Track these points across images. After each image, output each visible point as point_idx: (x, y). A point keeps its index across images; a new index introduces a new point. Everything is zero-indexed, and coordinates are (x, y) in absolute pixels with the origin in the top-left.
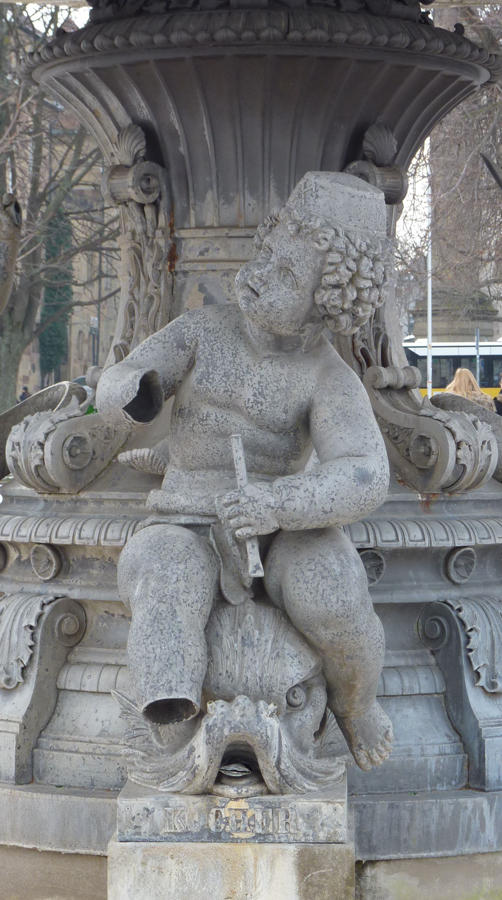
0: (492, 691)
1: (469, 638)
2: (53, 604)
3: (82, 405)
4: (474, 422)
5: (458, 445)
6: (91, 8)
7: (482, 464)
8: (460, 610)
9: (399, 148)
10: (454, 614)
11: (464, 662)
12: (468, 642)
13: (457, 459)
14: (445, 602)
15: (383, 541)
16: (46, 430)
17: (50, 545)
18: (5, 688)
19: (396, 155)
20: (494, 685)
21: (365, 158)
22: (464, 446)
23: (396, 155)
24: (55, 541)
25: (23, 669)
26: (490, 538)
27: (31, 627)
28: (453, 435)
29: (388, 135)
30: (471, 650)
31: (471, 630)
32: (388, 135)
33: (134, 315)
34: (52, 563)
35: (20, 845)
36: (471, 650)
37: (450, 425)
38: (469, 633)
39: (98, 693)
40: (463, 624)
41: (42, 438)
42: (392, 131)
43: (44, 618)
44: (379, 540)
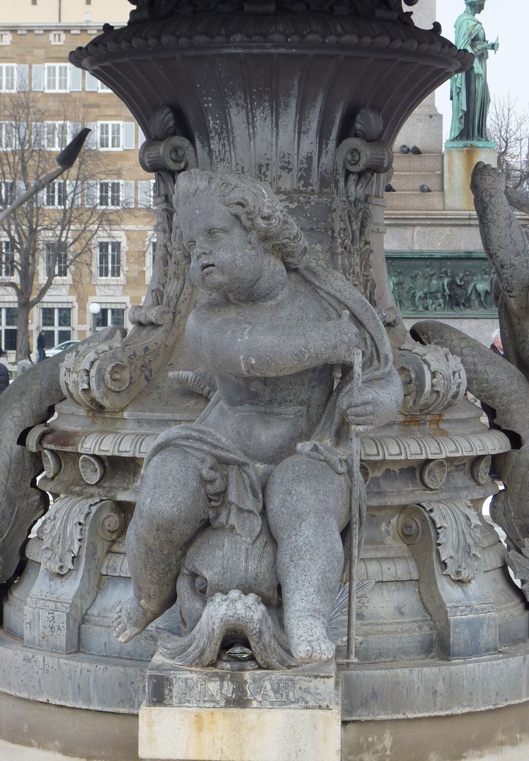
0: (457, 579)
1: (438, 534)
2: (99, 505)
3: (124, 339)
4: (446, 356)
5: (434, 375)
6: (134, 7)
7: (454, 389)
8: (431, 511)
9: (385, 126)
10: (426, 515)
11: (434, 553)
12: (438, 538)
13: (433, 386)
14: (419, 505)
15: (390, 455)
16: (91, 359)
17: (94, 456)
18: (58, 574)
19: (383, 131)
20: (458, 573)
21: (356, 136)
22: (439, 376)
23: (383, 131)
24: (96, 453)
25: (73, 558)
26: (472, 451)
27: (80, 524)
28: (429, 365)
29: (251, 122)
30: (439, 545)
31: (440, 528)
32: (251, 122)
33: (167, 264)
34: (97, 470)
35: (420, 715)
36: (439, 545)
37: (427, 358)
38: (439, 531)
39: (382, 582)
40: (434, 522)
41: (87, 367)
42: (379, 113)
43: (92, 515)
44: (428, 452)
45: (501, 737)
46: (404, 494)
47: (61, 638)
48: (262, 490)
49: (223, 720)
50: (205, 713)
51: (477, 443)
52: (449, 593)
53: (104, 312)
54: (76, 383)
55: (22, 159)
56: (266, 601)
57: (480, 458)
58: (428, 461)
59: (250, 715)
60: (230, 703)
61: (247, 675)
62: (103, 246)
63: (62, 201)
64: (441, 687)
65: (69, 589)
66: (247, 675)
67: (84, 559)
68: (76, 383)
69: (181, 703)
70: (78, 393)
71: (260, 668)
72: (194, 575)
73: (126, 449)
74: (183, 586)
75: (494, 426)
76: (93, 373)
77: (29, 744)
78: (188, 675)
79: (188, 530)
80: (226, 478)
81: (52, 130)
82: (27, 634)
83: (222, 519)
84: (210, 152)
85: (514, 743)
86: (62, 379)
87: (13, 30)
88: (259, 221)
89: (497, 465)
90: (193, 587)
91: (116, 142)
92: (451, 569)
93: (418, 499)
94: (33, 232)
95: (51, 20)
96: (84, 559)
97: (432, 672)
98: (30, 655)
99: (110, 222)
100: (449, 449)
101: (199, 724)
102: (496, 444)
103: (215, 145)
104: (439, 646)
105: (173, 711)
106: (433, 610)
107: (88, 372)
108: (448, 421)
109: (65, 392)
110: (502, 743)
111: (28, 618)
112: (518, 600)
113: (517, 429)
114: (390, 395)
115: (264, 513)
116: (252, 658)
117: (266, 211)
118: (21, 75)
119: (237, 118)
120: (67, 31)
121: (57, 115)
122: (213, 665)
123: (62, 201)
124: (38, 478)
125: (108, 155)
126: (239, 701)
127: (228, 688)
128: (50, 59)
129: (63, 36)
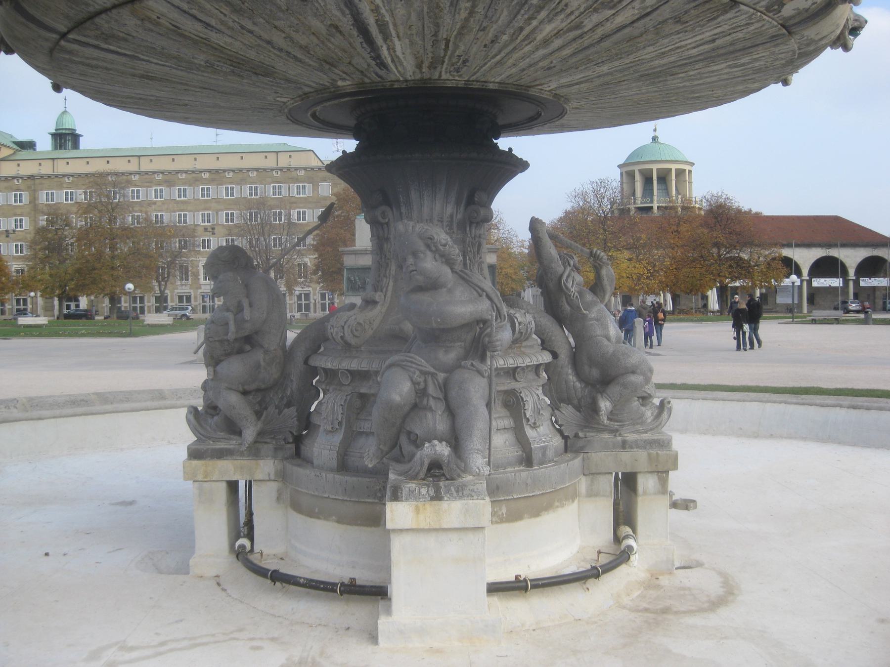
5: (520, 324)
45: (557, 504)
46: (507, 385)
47: (334, 463)
48: (445, 388)
49: (430, 508)
50: (420, 504)
51: (540, 359)
52: (530, 433)
53: (301, 294)
54: (337, 333)
55: (262, 227)
56: (449, 444)
57: (540, 364)
58: (517, 367)
59: (444, 505)
60: (433, 499)
61: (441, 484)
62: (299, 265)
63: (280, 245)
64: (529, 481)
65: (338, 438)
66: (441, 484)
67: (344, 423)
68: (337, 333)
69: (407, 500)
70: (338, 339)
71: (447, 479)
72: (409, 433)
73: (364, 366)
74: (403, 440)
75: (544, 348)
76: (346, 327)
77: (319, 518)
78: (410, 485)
79: (406, 409)
80: (425, 381)
81: (275, 213)
82: (315, 462)
83: (425, 402)
84: (401, 214)
85: (562, 506)
86: (329, 331)
87: (257, 170)
88: (441, 248)
89: (547, 367)
90: (409, 438)
91: (304, 219)
92: (532, 421)
93: (513, 387)
94: (268, 260)
95: (274, 165)
96: (344, 423)
97: (525, 474)
98: (318, 473)
99: (302, 255)
100: (528, 362)
101: (417, 510)
102: (546, 358)
103: (403, 210)
104: (527, 460)
105: (404, 503)
106: (522, 441)
107: (343, 328)
108: (525, 347)
109: (330, 337)
110: (557, 507)
111: (316, 454)
112: (559, 435)
113: (556, 350)
114: (505, 335)
115: (446, 398)
116: (444, 475)
117: (444, 242)
118: (261, 190)
119: (414, 195)
120: (281, 169)
121: (277, 207)
122: (423, 479)
123: (280, 245)
124: (314, 381)
125: (302, 224)
126: (437, 497)
127: (432, 493)
128: (273, 182)
129: (279, 172)
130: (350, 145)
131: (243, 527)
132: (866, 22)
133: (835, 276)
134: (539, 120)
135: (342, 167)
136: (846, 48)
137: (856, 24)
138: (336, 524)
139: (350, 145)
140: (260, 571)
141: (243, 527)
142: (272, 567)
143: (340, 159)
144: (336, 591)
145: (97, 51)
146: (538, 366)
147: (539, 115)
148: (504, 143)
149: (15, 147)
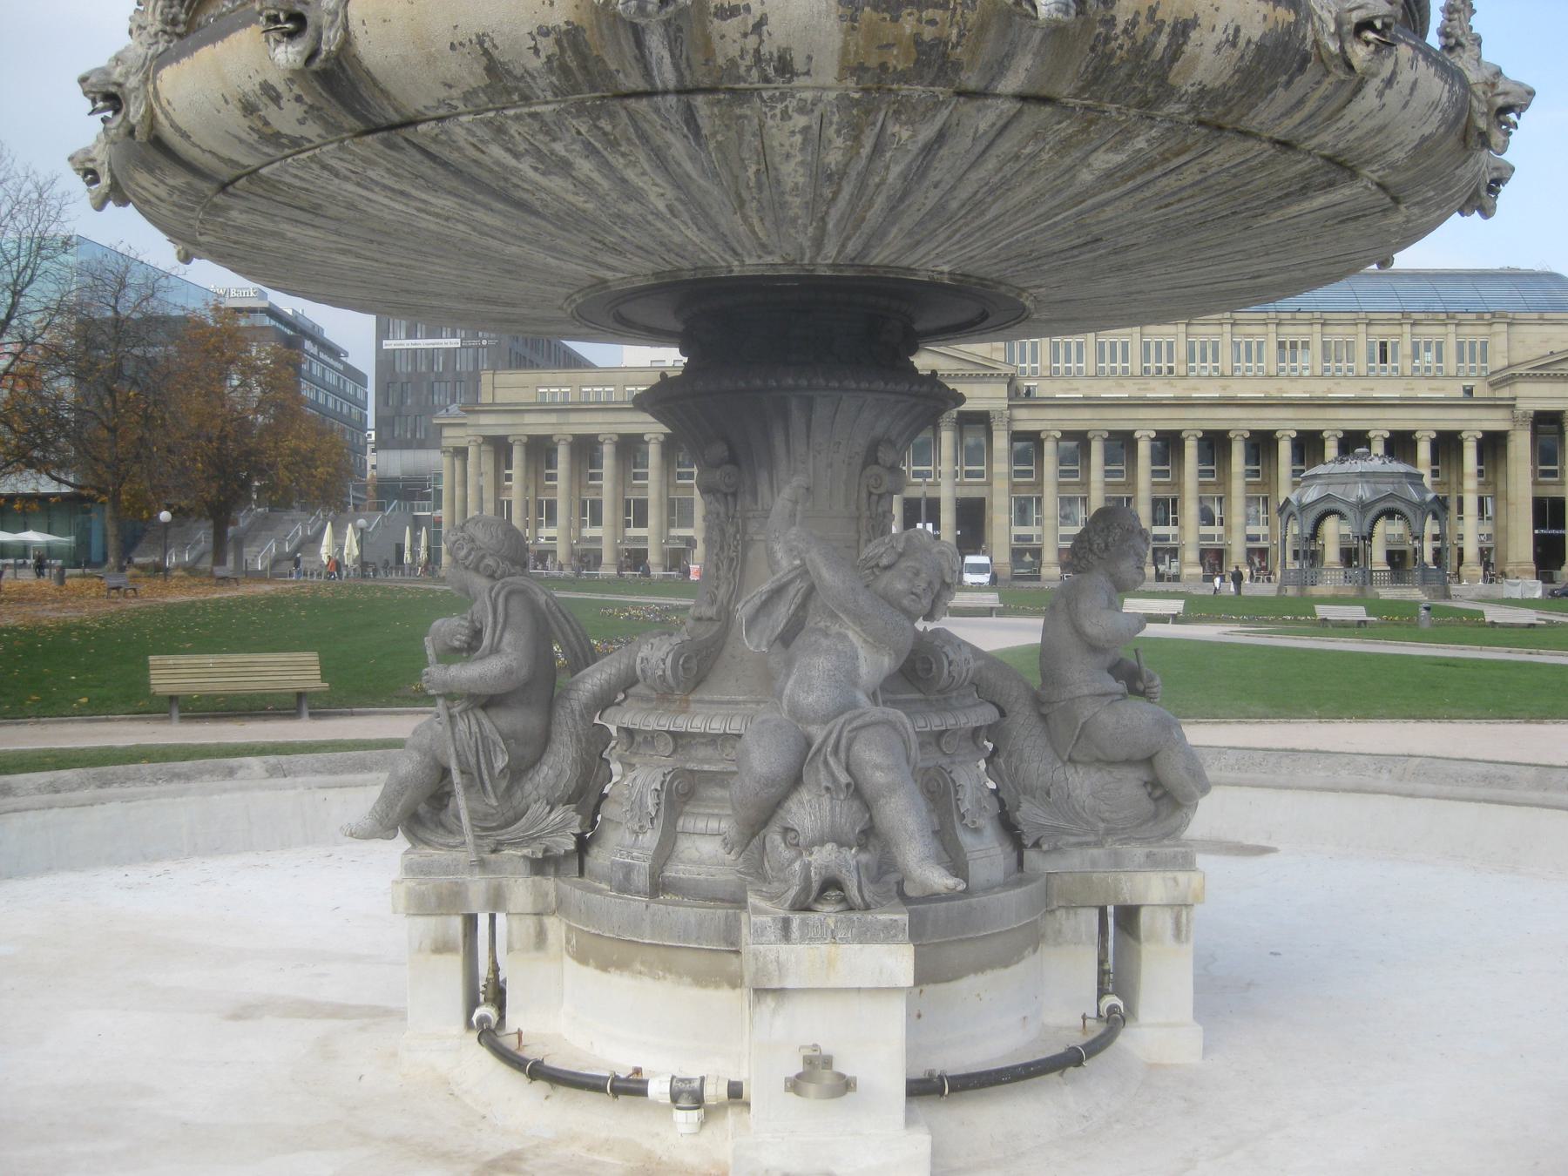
5: (950, 663)
89: (992, 731)
130: (671, 357)
131: (487, 995)
132: (1513, 169)
133: (984, 553)
134: (985, 324)
135: (661, 397)
136: (1487, 212)
137: (1495, 175)
138: (598, 973)
139: (671, 357)
140: (512, 1059)
141: (487, 995)
142: (109, 805)
143: (654, 389)
144: (604, 1091)
145: (428, 162)
146: (976, 731)
147: (984, 316)
148: (924, 361)
149: (1374, 188)
